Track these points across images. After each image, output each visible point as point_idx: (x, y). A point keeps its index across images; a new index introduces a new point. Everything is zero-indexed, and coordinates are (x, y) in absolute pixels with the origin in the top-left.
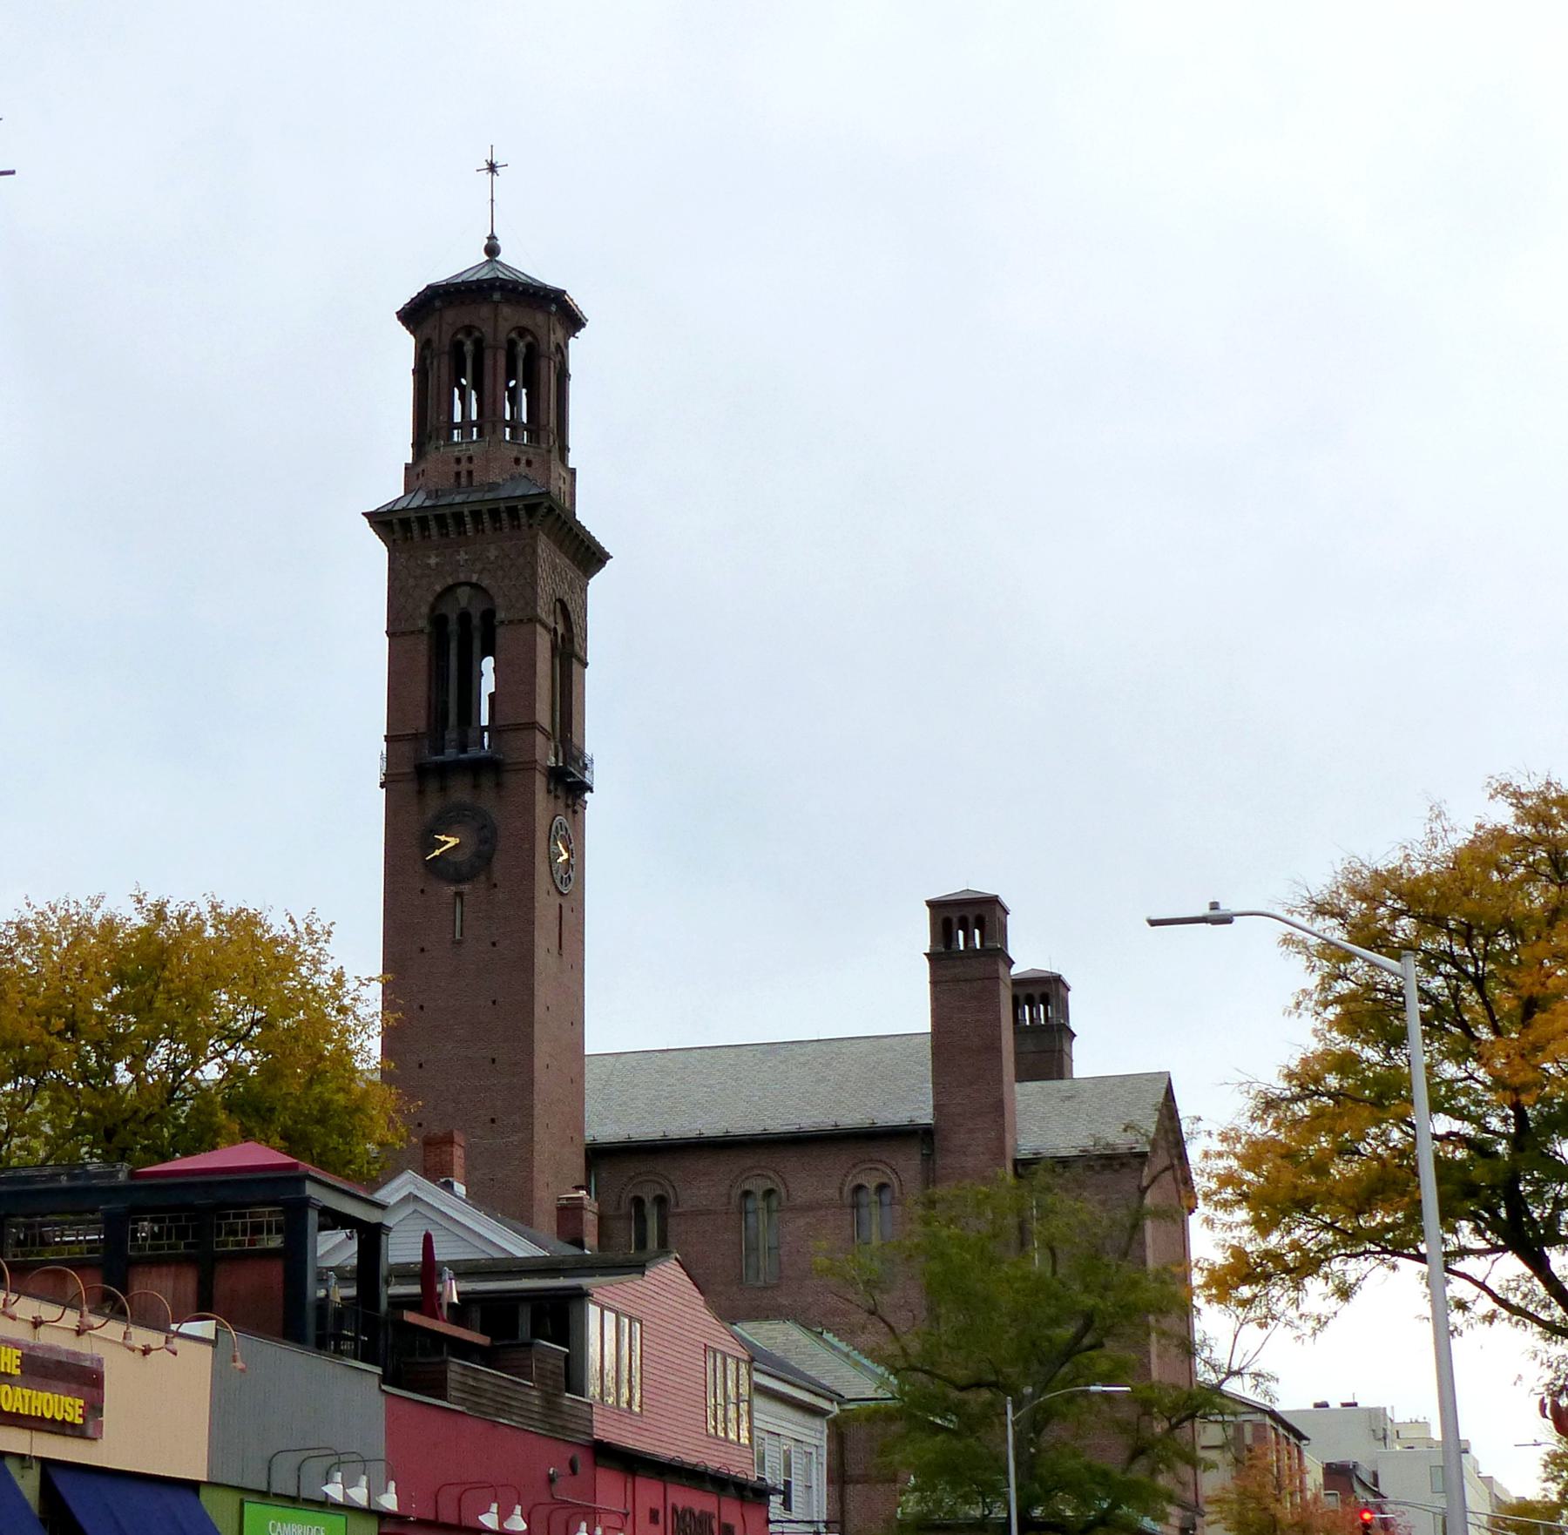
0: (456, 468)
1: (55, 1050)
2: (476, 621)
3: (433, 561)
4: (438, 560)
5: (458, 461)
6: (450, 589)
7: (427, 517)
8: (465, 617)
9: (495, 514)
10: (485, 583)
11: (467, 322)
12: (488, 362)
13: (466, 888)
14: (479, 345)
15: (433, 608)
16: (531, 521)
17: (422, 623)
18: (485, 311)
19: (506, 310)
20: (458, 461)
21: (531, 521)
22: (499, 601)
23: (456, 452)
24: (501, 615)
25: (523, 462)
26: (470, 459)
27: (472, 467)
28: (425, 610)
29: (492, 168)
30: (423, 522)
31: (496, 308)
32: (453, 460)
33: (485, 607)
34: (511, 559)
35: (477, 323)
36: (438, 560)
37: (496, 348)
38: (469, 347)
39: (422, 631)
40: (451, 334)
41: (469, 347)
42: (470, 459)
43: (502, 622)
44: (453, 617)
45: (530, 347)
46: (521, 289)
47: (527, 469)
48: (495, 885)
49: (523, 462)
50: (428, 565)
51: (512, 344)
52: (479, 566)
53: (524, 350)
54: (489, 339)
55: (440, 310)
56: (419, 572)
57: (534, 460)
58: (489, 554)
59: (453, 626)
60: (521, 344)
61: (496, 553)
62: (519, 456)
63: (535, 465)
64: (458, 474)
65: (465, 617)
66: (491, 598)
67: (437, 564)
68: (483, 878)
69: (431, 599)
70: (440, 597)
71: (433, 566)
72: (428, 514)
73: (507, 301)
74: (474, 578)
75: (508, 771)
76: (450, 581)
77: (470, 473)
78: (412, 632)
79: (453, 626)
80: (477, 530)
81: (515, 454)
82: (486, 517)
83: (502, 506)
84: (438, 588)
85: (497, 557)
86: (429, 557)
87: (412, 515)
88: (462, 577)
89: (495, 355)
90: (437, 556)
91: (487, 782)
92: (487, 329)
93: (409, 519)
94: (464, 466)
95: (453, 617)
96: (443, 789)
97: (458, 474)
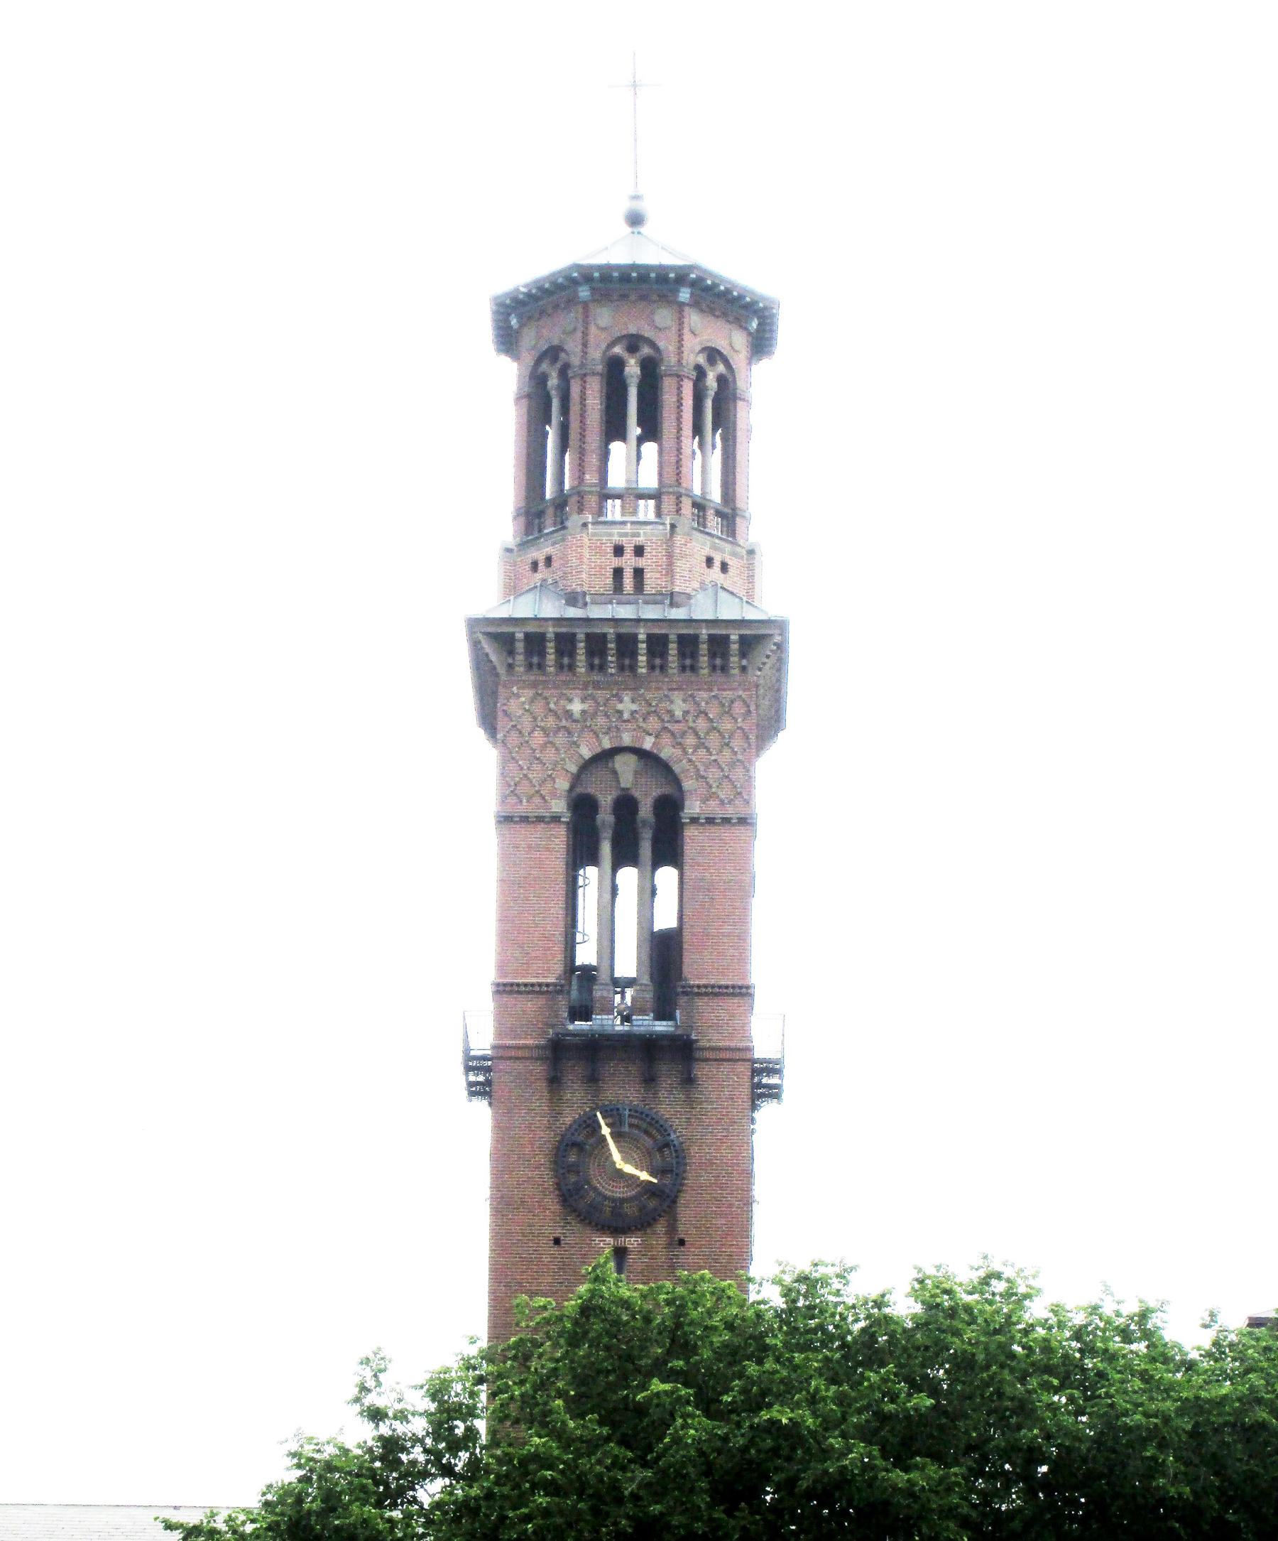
0: (616, 562)
1: (730, 1319)
2: (645, 811)
3: (577, 707)
4: (585, 706)
5: (619, 551)
6: (604, 757)
7: (574, 635)
8: (626, 805)
9: (688, 644)
10: (667, 753)
11: (632, 330)
12: (668, 398)
13: (632, 1242)
14: (651, 370)
15: (576, 780)
16: (744, 662)
17: (559, 806)
18: (664, 316)
19: (694, 318)
20: (619, 551)
21: (744, 662)
22: (688, 784)
23: (616, 536)
24: (693, 807)
25: (717, 564)
26: (639, 551)
27: (641, 562)
28: (563, 784)
29: (635, 85)
30: (566, 643)
31: (681, 312)
32: (610, 550)
33: (667, 790)
34: (711, 720)
35: (648, 333)
36: (585, 706)
37: (680, 377)
38: (633, 369)
39: (556, 819)
40: (604, 346)
41: (633, 369)
42: (639, 551)
43: (694, 820)
44: (606, 800)
45: (721, 380)
46: (653, 275)
47: (722, 575)
48: (682, 1242)
49: (717, 564)
50: (569, 714)
51: (700, 373)
52: (653, 723)
53: (715, 385)
54: (670, 359)
55: (585, 305)
56: (551, 722)
57: (730, 562)
58: (673, 707)
59: (605, 817)
60: (632, 361)
61: (685, 706)
62: (713, 554)
63: (732, 571)
64: (618, 573)
65: (626, 805)
66: (676, 781)
67: (583, 712)
68: (660, 1228)
69: (574, 769)
70: (588, 765)
71: (577, 715)
72: (577, 630)
73: (696, 304)
74: (648, 744)
75: (707, 1060)
76: (607, 744)
77: (639, 573)
78: (540, 819)
79: (605, 817)
80: (652, 667)
81: (707, 551)
82: (673, 648)
83: (704, 632)
84: (586, 753)
85: (686, 713)
86: (570, 701)
87: (610, 631)
88: (627, 740)
89: (679, 388)
90: (583, 700)
91: (668, 1076)
92: (667, 345)
93: (605, 635)
94: (628, 562)
95: (606, 800)
96: (593, 1079)
97: (618, 573)
